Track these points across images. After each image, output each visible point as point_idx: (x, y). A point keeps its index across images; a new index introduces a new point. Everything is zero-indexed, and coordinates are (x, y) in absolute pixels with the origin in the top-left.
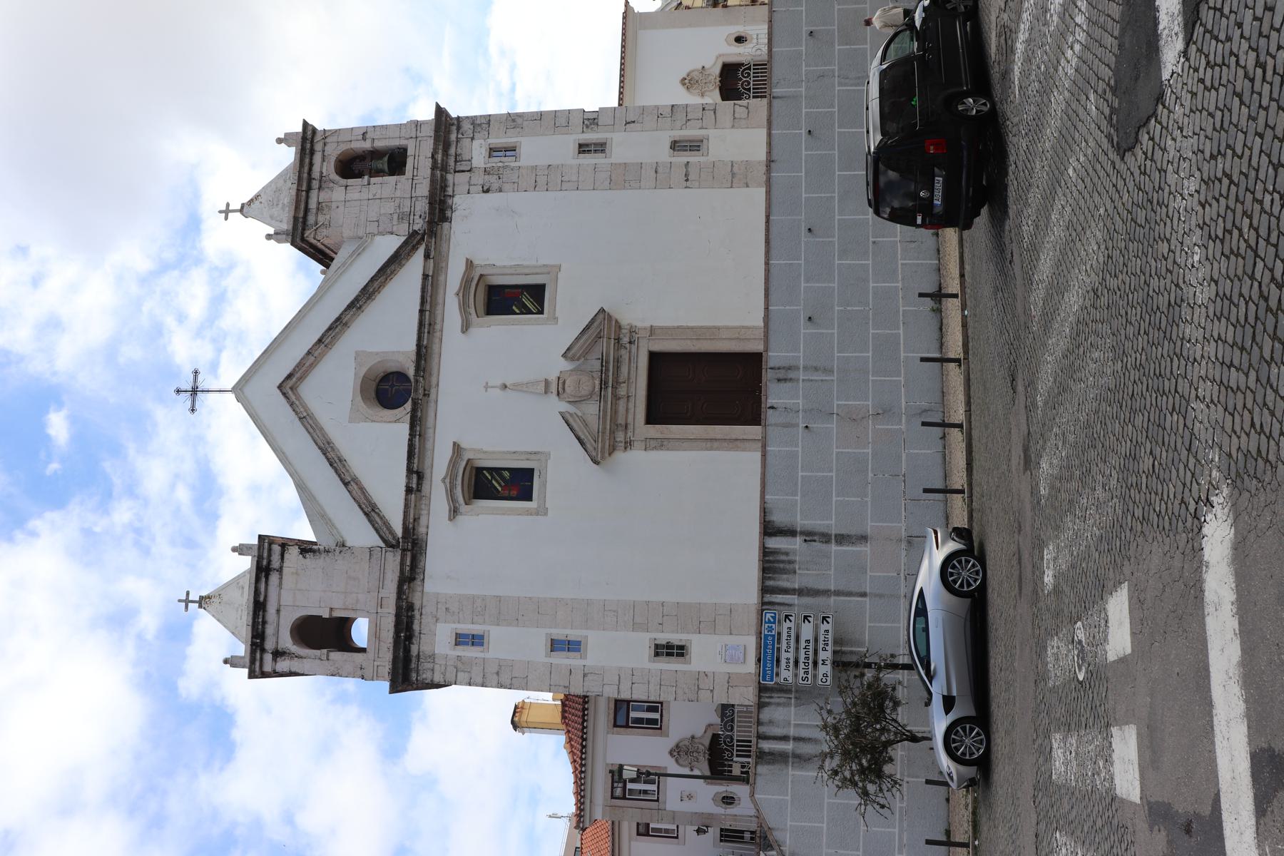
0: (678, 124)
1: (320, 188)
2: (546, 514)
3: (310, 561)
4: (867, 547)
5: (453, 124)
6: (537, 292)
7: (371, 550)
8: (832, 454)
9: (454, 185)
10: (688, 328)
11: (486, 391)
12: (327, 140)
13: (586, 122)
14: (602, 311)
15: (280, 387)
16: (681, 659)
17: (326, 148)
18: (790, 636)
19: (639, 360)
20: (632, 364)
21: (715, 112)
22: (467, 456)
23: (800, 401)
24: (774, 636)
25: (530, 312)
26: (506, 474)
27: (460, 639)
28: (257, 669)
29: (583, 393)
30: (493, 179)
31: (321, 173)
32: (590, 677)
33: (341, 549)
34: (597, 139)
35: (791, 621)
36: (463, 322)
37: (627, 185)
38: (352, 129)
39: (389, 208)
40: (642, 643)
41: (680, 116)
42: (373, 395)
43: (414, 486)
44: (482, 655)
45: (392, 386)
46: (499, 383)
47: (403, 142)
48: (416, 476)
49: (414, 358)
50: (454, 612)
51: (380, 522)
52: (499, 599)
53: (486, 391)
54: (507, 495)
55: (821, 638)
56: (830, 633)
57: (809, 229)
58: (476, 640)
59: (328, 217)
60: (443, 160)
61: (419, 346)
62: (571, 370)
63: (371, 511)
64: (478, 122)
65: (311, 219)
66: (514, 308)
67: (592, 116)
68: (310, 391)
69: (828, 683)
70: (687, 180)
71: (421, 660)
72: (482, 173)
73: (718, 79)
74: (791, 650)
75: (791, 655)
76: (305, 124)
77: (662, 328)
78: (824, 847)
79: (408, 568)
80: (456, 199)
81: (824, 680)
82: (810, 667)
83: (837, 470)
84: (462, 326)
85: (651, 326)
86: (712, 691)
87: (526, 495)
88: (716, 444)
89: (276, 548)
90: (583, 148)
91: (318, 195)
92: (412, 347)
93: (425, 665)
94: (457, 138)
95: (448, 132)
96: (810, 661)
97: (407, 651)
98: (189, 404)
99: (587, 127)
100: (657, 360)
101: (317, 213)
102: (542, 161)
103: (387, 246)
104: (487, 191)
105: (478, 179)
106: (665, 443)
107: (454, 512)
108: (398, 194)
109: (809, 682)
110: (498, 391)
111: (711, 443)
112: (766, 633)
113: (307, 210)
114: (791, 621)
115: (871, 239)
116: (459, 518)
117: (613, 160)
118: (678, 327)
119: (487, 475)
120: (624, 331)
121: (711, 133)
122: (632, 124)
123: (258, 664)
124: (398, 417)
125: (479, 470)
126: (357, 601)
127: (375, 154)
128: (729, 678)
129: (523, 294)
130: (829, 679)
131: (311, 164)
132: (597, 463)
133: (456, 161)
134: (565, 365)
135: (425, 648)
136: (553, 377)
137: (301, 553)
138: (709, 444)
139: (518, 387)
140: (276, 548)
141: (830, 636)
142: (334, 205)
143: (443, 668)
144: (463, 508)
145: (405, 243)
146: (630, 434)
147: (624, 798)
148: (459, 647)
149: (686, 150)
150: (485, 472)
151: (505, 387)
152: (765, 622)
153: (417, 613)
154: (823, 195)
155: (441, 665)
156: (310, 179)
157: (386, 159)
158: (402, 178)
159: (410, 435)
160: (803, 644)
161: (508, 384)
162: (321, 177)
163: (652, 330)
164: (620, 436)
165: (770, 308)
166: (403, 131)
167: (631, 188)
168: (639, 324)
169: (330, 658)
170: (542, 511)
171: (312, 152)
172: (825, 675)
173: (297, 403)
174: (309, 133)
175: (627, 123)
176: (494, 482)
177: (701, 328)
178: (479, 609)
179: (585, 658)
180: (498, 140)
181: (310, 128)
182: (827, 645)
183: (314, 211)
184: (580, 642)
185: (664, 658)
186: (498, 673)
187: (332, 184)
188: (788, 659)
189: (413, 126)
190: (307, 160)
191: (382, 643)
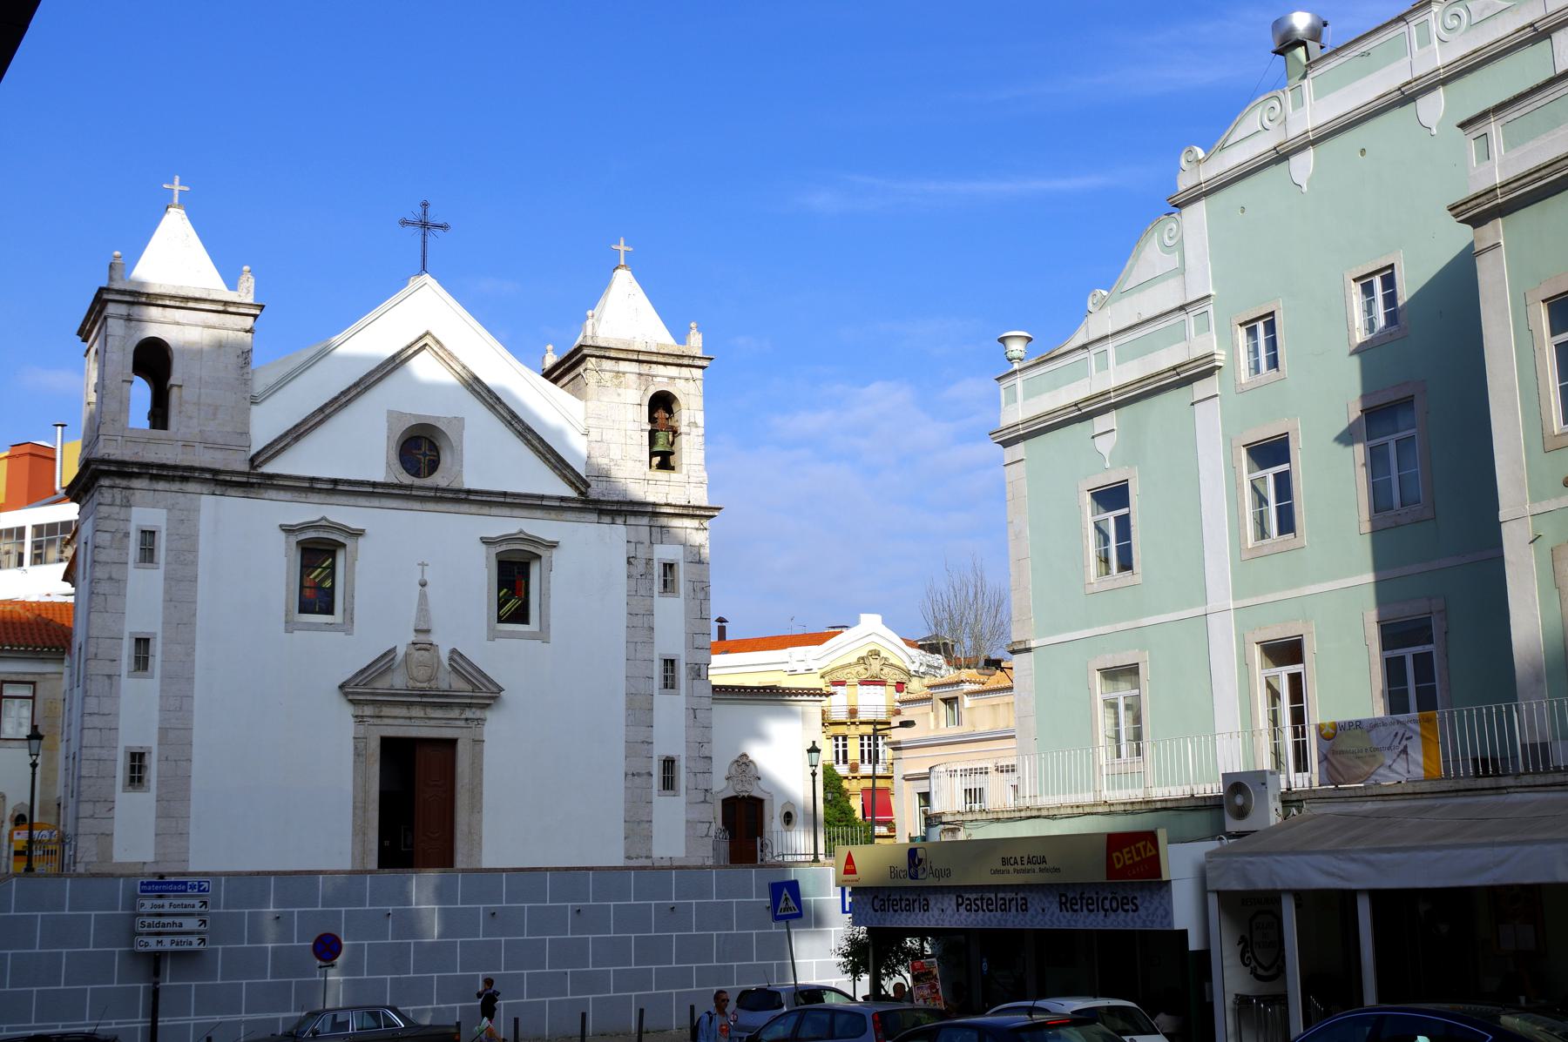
2: (287, 631)
6: (521, 616)
7: (247, 433)
11: (419, 564)
13: (697, 667)
16: (128, 780)
20: (444, 722)
21: (703, 802)
22: (348, 542)
25: (500, 607)
26: (328, 584)
27: (148, 535)
32: (107, 681)
33: (248, 399)
34: (679, 679)
35: (201, 907)
41: (701, 766)
45: (425, 455)
46: (427, 578)
47: (685, 471)
48: (335, 488)
49: (455, 485)
52: (194, 579)
53: (419, 564)
55: (184, 938)
58: (147, 553)
59: (609, 384)
61: (469, 492)
63: (297, 433)
65: (607, 364)
66: (505, 590)
67: (703, 672)
69: (139, 948)
70: (633, 775)
72: (648, 556)
73: (746, 794)
74: (172, 910)
75: (167, 909)
81: (142, 943)
85: (483, 741)
86: (92, 817)
90: (670, 664)
96: (160, 929)
99: (692, 668)
102: (658, 622)
104: (629, 563)
105: (642, 553)
107: (288, 530)
109: (140, 929)
110: (420, 577)
114: (201, 907)
116: (283, 535)
119: (327, 563)
121: (681, 800)
124: (392, 466)
125: (333, 554)
126: (191, 418)
128: (108, 835)
130: (142, 948)
136: (433, 638)
139: (423, 598)
144: (294, 539)
145: (578, 476)
148: (139, 534)
149: (664, 773)
150: (330, 560)
151: (423, 585)
153: (176, 486)
159: (374, 482)
160: (177, 920)
161: (426, 588)
162: (653, 376)
163: (479, 742)
164: (368, 710)
172: (147, 944)
175: (694, 710)
176: (320, 570)
178: (182, 558)
179: (129, 677)
182: (177, 945)
183: (616, 369)
187: (643, 388)
191: (142, 445)
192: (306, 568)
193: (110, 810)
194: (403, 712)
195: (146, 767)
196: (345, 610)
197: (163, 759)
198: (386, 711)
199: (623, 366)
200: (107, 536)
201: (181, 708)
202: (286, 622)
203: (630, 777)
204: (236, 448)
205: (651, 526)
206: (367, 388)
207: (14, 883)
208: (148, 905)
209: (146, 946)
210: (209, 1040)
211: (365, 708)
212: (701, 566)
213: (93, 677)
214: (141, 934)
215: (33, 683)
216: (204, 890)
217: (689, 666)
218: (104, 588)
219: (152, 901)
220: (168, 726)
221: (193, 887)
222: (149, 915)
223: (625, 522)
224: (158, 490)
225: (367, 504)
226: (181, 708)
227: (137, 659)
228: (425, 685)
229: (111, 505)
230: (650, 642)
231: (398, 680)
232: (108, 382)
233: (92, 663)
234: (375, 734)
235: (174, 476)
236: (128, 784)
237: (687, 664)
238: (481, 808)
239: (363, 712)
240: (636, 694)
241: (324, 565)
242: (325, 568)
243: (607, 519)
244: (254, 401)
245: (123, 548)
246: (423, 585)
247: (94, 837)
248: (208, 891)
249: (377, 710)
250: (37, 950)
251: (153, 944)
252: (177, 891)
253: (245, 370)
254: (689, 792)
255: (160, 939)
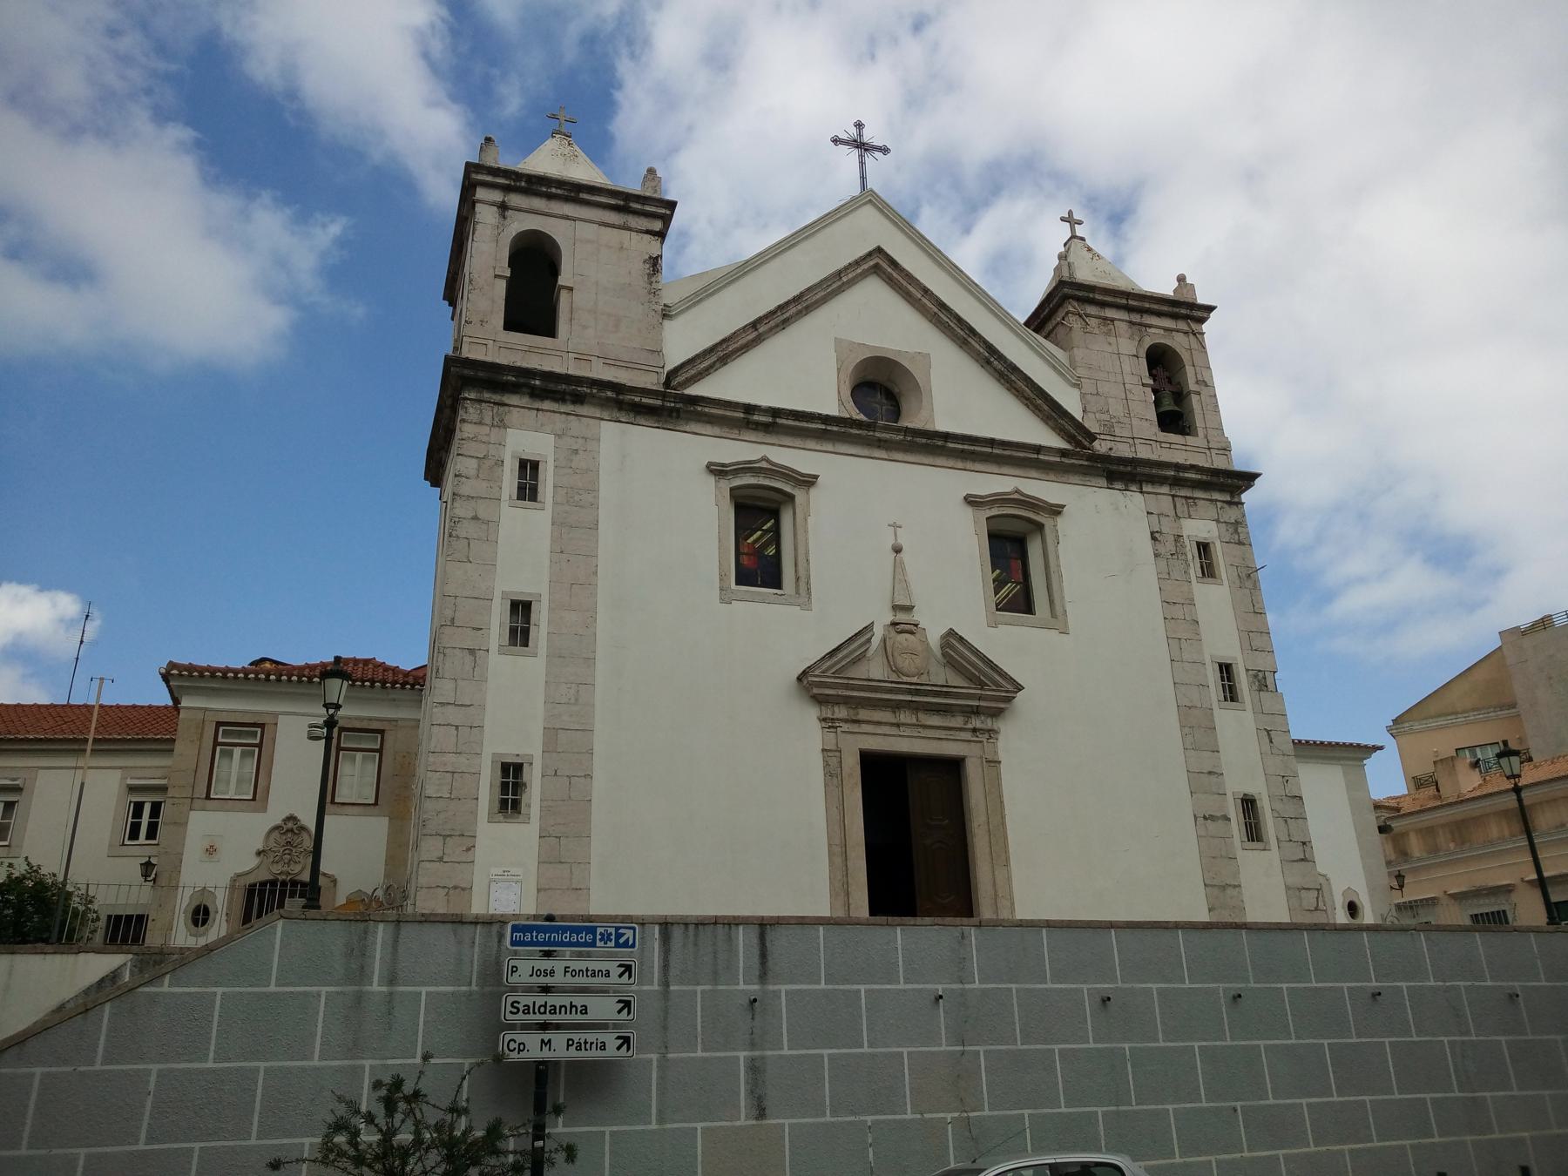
0: (1278, 806)
1: (1130, 322)
2: (722, 601)
3: (639, 268)
4: (747, 1118)
5: (1232, 496)
7: (659, 352)
8: (899, 1046)
9: (1156, 494)
10: (1003, 817)
12: (1191, 336)
13: (1261, 675)
14: (1019, 688)
15: (879, 250)
16: (497, 805)
17: (1182, 334)
18: (593, 975)
19: (951, 743)
21: (1302, 860)
22: (799, 494)
23: (977, 985)
24: (593, 944)
26: (771, 551)
27: (528, 468)
28: (480, 177)
29: (899, 660)
30: (1170, 546)
31: (1150, 326)
32: (468, 659)
34: (1241, 690)
36: (981, 497)
37: (1187, 730)
38: (1209, 368)
39: (1117, 409)
40: (527, 744)
41: (1289, 809)
42: (870, 378)
43: (756, 418)
44: (505, 495)
47: (1201, 432)
49: (929, 427)
50: (571, 461)
51: (702, 366)
52: (595, 526)
54: (741, 550)
55: (591, 1036)
56: (600, 1053)
57: (1240, 996)
58: (528, 491)
60: (1187, 480)
61: (947, 436)
62: (928, 644)
63: (723, 353)
64: (1240, 530)
65: (1092, 310)
67: (1269, 681)
68: (873, 291)
70: (1205, 818)
71: (496, 408)
75: (559, 979)
76: (1210, 309)
77: (999, 774)
78: (162, 1066)
79: (637, 399)
80: (1138, 497)
82: (538, 1016)
83: (873, 1056)
84: (976, 496)
86: (441, 859)
87: (744, 578)
88: (838, 860)
89: (657, 225)
90: (1226, 670)
91: (1122, 320)
92: (942, 425)
93: (488, 413)
94: (1216, 500)
95: (1222, 488)
96: (548, 1017)
97: (514, 389)
98: (844, 136)
99: (1256, 676)
100: (953, 768)
101: (1100, 317)
102: (1202, 613)
103: (1070, 401)
104: (1154, 538)
106: (835, 780)
108: (1135, 422)
109: (509, 1016)
110: (890, 542)
111: (838, 851)
112: (599, 930)
113: (1103, 305)
114: (621, 975)
115: (1238, 1104)
116: (712, 479)
117: (1217, 712)
118: (1002, 802)
119: (769, 525)
120: (989, 721)
122: (1268, 741)
123: (489, 178)
125: (775, 514)
126: (585, 327)
127: (1181, 396)
128: (463, 889)
129: (1018, 583)
131: (1159, 314)
132: (799, 679)
133: (1186, 498)
134: (934, 636)
135: (515, 415)
136: (916, 616)
137: (650, 257)
138: (837, 850)
139: (898, 568)
140: (657, 225)
141: (594, 1054)
142: (1112, 340)
143: (485, 439)
144: (726, 485)
146: (846, 727)
147: (216, 743)
152: (617, 929)
153: (569, 408)
154: (1290, 1018)
155: (488, 435)
156: (1142, 311)
157: (1176, 408)
158: (1156, 428)
160: (579, 1001)
161: (901, 555)
164: (841, 712)
165: (1113, 931)
166: (1215, 433)
167: (1184, 736)
168: (1001, 744)
169: (497, 280)
170: (726, 599)
171: (1175, 317)
172: (522, 1047)
173: (859, 271)
174: (1200, 314)
175: (1268, 731)
176: (759, 533)
177: (1006, 838)
180: (1219, 552)
181: (1205, 315)
182: (579, 1048)
183: (1103, 314)
184: (527, 646)
185: (499, 779)
186: (475, 518)
188: (552, 973)
189: (1224, 445)
190: (1165, 308)
192: (742, 531)
193: (468, 849)
194: (886, 716)
195: (525, 785)
196: (798, 579)
197: (551, 774)
198: (864, 714)
199: (1110, 313)
200: (473, 463)
201: (577, 700)
202: (721, 589)
203: (1201, 820)
204: (647, 368)
205: (1173, 496)
206: (808, 309)
207: (279, 929)
208: (526, 968)
209: (520, 1051)
210: (1526, 1174)
211: (836, 709)
212: (1242, 547)
213: (447, 651)
214: (512, 1027)
215: (382, 732)
216: (626, 944)
217: (1251, 672)
218: (465, 529)
219: (532, 963)
220: (558, 726)
221: (606, 938)
222: (529, 990)
223: (1142, 489)
224: (542, 410)
225: (818, 448)
226: (577, 700)
227: (513, 631)
228: (915, 680)
229: (480, 423)
230: (1197, 637)
231: (876, 670)
232: (476, 276)
233: (448, 630)
234: (855, 743)
235: (564, 393)
236: (496, 810)
237: (1247, 670)
238: (1008, 859)
239: (833, 713)
240: (1190, 708)
241: (765, 528)
242: (766, 532)
243: (1119, 485)
244: (666, 314)
245: (495, 480)
246: (897, 550)
247: (442, 892)
248: (633, 946)
249: (851, 711)
250: (316, 1062)
251: (533, 1048)
252: (578, 944)
253: (653, 279)
254: (1281, 844)
255: (546, 1037)
